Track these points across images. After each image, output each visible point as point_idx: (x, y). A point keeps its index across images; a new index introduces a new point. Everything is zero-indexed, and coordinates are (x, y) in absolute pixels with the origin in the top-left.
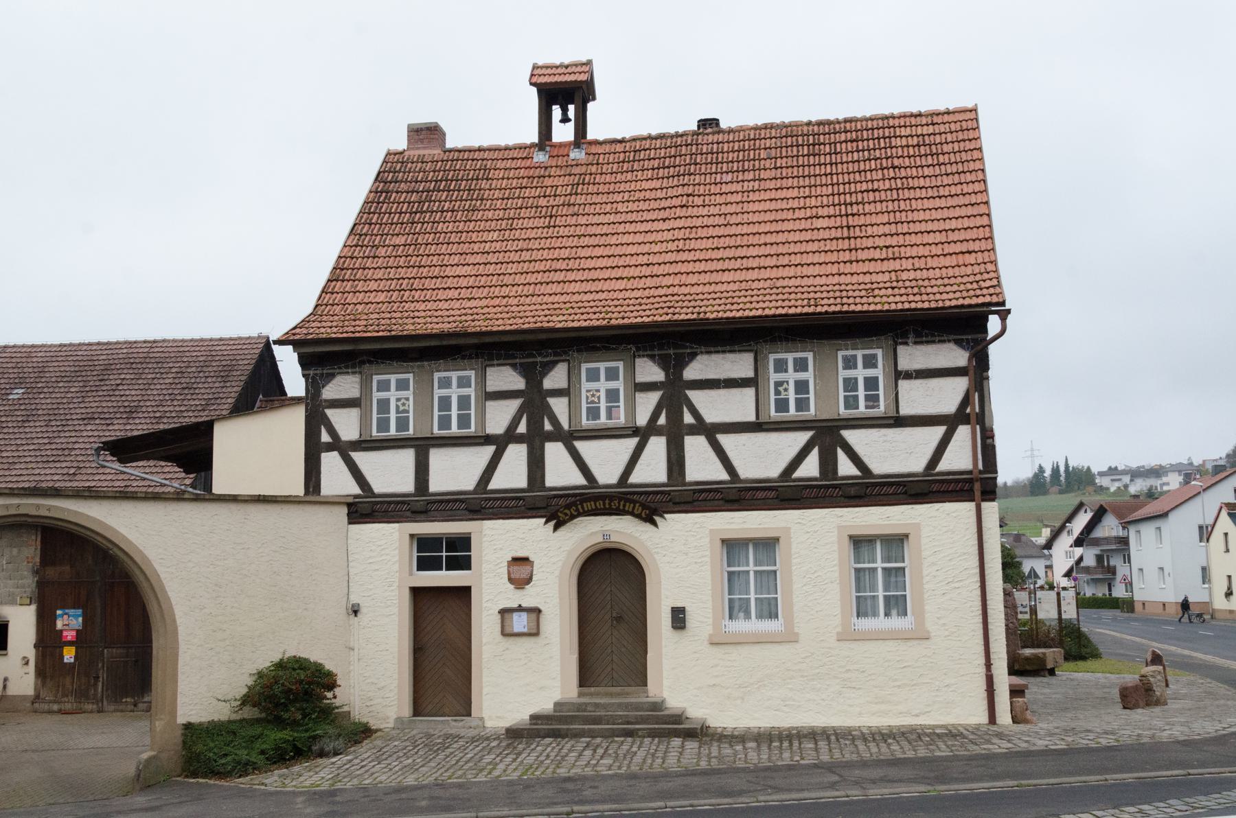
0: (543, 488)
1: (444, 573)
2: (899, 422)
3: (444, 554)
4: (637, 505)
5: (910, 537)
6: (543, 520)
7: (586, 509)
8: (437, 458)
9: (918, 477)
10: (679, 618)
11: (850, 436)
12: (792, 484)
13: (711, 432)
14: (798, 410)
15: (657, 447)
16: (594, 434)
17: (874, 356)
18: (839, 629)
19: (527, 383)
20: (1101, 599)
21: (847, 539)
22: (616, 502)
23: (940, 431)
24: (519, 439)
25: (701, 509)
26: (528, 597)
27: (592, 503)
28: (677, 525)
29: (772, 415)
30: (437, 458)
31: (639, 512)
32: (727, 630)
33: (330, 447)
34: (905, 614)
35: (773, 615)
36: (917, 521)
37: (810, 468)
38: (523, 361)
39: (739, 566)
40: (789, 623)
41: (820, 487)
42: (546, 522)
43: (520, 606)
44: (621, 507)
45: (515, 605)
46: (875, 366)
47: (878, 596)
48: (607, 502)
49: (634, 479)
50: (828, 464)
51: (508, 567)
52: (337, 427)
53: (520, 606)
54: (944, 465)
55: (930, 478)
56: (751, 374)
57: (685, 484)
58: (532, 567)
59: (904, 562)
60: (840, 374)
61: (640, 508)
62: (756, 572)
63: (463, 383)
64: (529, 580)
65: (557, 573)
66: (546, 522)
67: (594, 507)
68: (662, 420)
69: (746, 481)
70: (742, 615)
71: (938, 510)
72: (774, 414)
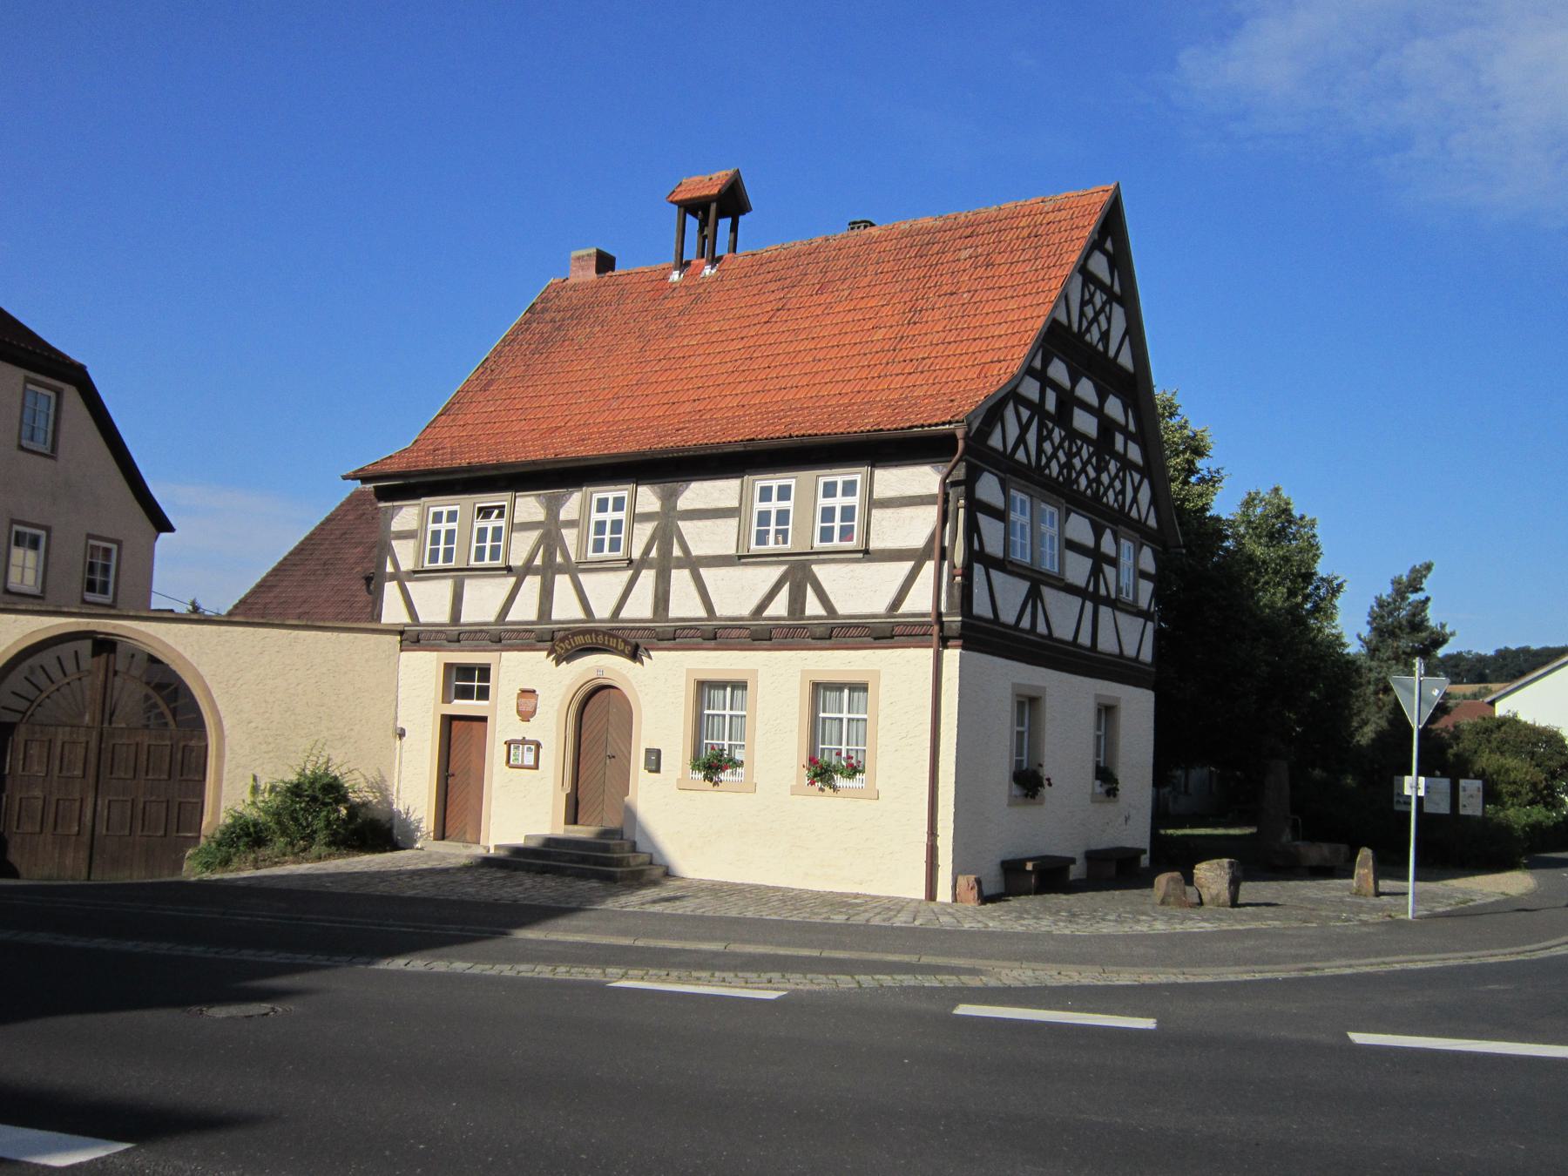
0: (550, 622)
1: (474, 702)
2: (867, 554)
3: (476, 684)
4: (620, 640)
6: (545, 653)
7: (615, 640)
8: (471, 588)
9: (881, 618)
10: (654, 761)
11: (820, 571)
12: (763, 623)
13: (694, 564)
15: (648, 578)
18: (794, 783)
19: (662, 505)
22: (601, 636)
23: (908, 566)
25: (800, 647)
26: (530, 731)
27: (582, 637)
28: (660, 660)
29: (815, 546)
30: (471, 588)
31: (622, 648)
33: (680, 564)
36: (876, 668)
37: (779, 607)
39: (858, 713)
41: (789, 627)
42: (548, 655)
43: (524, 738)
44: (606, 643)
45: (520, 738)
48: (593, 635)
49: (624, 614)
50: (797, 602)
51: (518, 699)
53: (524, 738)
54: (905, 608)
55: (893, 620)
56: (735, 504)
57: (668, 620)
58: (537, 700)
60: (592, 517)
61: (623, 644)
63: (849, 488)
64: (533, 713)
65: (556, 707)
66: (548, 655)
67: (614, 645)
68: (654, 553)
69: (721, 619)
71: (898, 656)
72: (754, 548)
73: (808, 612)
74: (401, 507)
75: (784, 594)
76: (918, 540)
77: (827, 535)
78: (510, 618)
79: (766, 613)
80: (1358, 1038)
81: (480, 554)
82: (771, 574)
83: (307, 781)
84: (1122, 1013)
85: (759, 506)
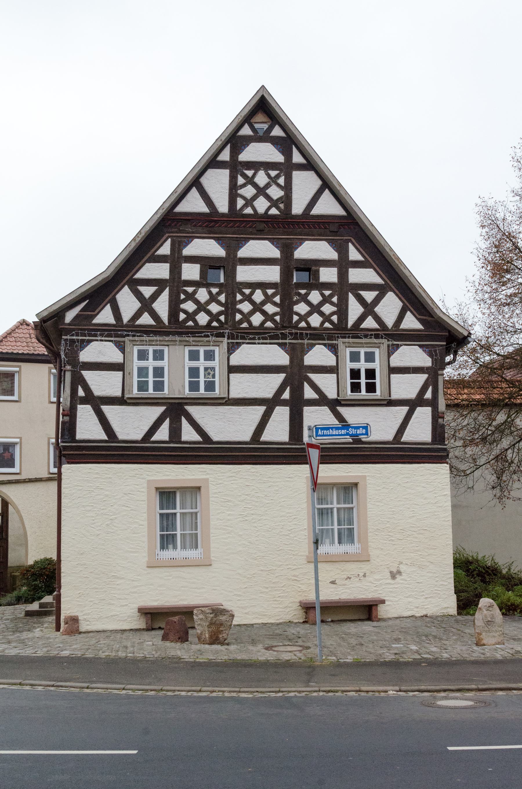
5: (202, 489)
11: (191, 409)
14: (206, 390)
16: (353, 403)
17: (162, 352)
20: (367, 535)
21: (154, 490)
24: (284, 403)
32: (159, 558)
33: (84, 401)
34: (197, 547)
35: (352, 541)
38: (290, 341)
40: (365, 548)
46: (162, 359)
47: (176, 534)
52: (89, 382)
54: (266, 437)
59: (352, 503)
62: (181, 513)
70: (171, 546)
73: (184, 438)
74: (89, 342)
75: (166, 425)
76: (412, 394)
77: (194, 386)
78: (404, 439)
79: (154, 438)
80: (450, 748)
81: (194, 386)
82: (158, 411)
83: (181, 633)
84: (6, 755)
85: (351, 365)
